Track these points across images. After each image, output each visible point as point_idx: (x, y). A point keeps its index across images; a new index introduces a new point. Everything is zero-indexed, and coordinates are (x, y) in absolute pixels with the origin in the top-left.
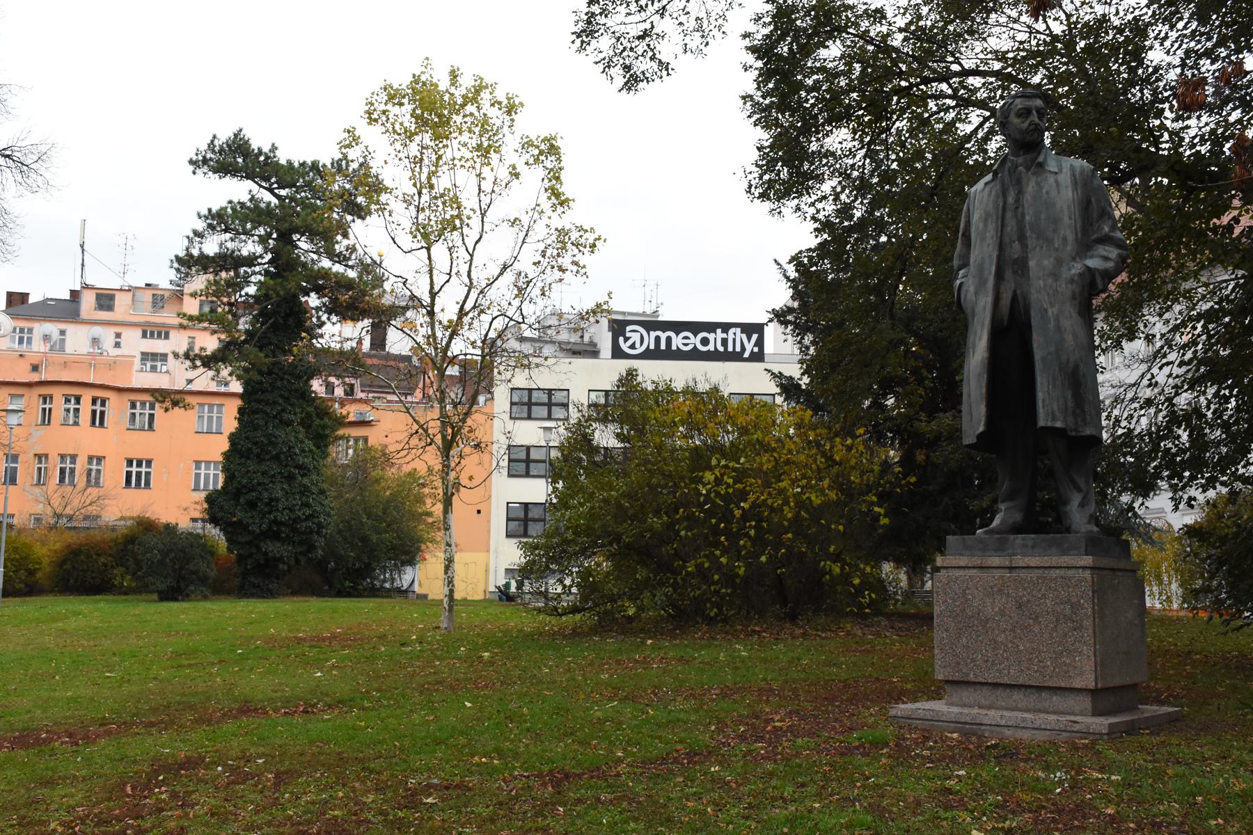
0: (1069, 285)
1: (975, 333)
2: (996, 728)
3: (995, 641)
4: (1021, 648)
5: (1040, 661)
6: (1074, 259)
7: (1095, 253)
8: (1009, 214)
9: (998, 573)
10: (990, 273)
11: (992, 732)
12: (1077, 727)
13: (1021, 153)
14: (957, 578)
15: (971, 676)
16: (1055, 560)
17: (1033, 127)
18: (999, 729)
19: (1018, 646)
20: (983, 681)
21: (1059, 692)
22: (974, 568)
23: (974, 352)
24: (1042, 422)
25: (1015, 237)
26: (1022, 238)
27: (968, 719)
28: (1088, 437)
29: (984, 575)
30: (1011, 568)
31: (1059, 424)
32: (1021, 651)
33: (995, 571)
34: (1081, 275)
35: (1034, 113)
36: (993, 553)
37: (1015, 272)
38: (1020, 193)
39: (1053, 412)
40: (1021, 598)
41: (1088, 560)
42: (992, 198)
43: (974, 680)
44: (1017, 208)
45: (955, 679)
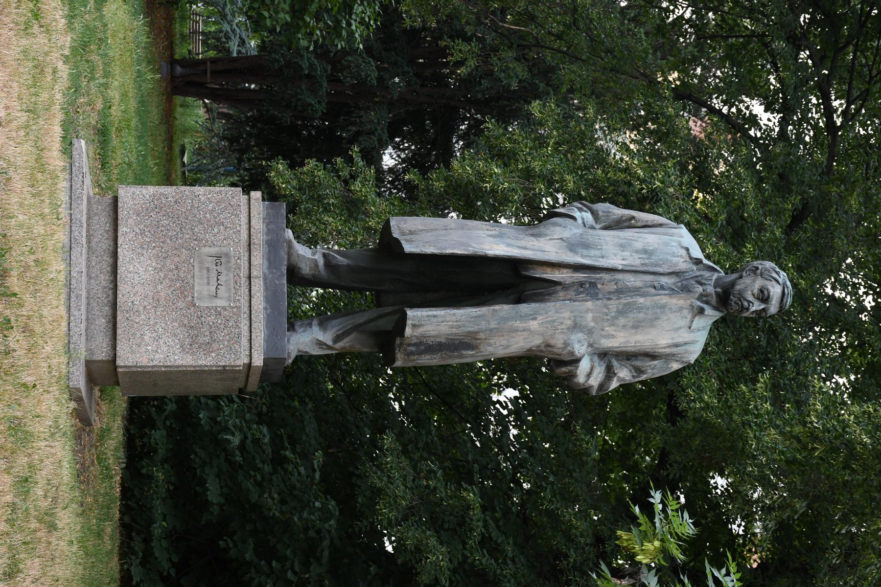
0: (562, 342)
1: (517, 239)
6: (590, 345)
7: (596, 364)
8: (649, 278)
14: (237, 216)
15: (125, 229)
17: (746, 304)
20: (119, 243)
21: (110, 325)
23: (494, 236)
24: (410, 313)
26: (620, 292)
28: (394, 354)
31: (408, 331)
33: (246, 258)
34: (572, 353)
35: (763, 306)
38: (672, 292)
41: (258, 361)
44: (655, 287)
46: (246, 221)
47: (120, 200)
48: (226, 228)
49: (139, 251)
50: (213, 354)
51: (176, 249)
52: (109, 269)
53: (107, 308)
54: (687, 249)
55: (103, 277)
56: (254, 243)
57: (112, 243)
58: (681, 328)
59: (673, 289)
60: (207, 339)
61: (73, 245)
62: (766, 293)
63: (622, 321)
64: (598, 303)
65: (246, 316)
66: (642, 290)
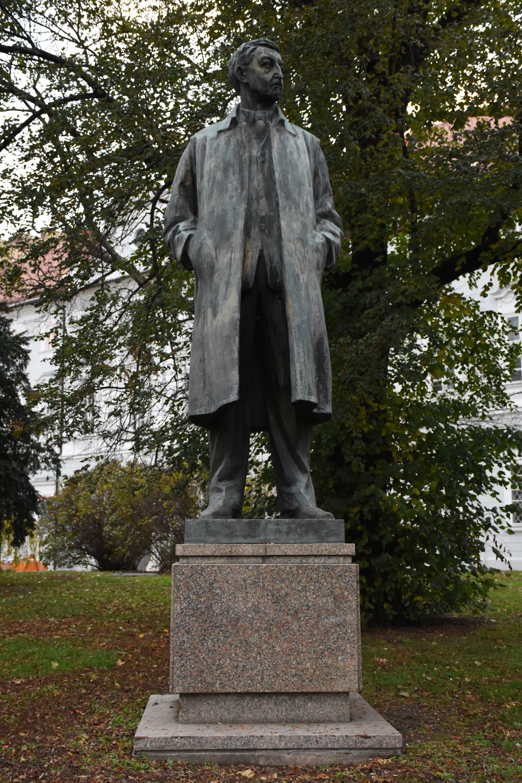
2: (272, 753)
3: (247, 643)
4: (278, 649)
5: (298, 664)
9: (251, 563)
10: (235, 227)
11: (268, 758)
12: (368, 743)
13: (259, 106)
14: (203, 570)
15: (217, 685)
16: (316, 548)
17: (276, 81)
18: (276, 754)
19: (273, 647)
20: (231, 690)
21: (314, 697)
22: (221, 556)
25: (262, 193)
27: (239, 745)
29: (235, 565)
30: (265, 557)
32: (278, 653)
33: (245, 560)
36: (242, 540)
37: (262, 231)
39: (309, 386)
40: (279, 591)
41: (350, 548)
42: (232, 147)
43: (220, 690)
45: (197, 691)
46: (206, 560)
47: (186, 691)
48: (215, 580)
49: (240, 670)
50: (346, 593)
51: (238, 632)
52: (256, 700)
53: (297, 701)
54: (220, 132)
55: (264, 706)
56: (230, 552)
57: (229, 698)
58: (296, 144)
59: (264, 145)
60: (330, 600)
61: (251, 747)
62: (266, 61)
63: (295, 196)
64: (281, 215)
65: (304, 561)
66: (266, 174)
